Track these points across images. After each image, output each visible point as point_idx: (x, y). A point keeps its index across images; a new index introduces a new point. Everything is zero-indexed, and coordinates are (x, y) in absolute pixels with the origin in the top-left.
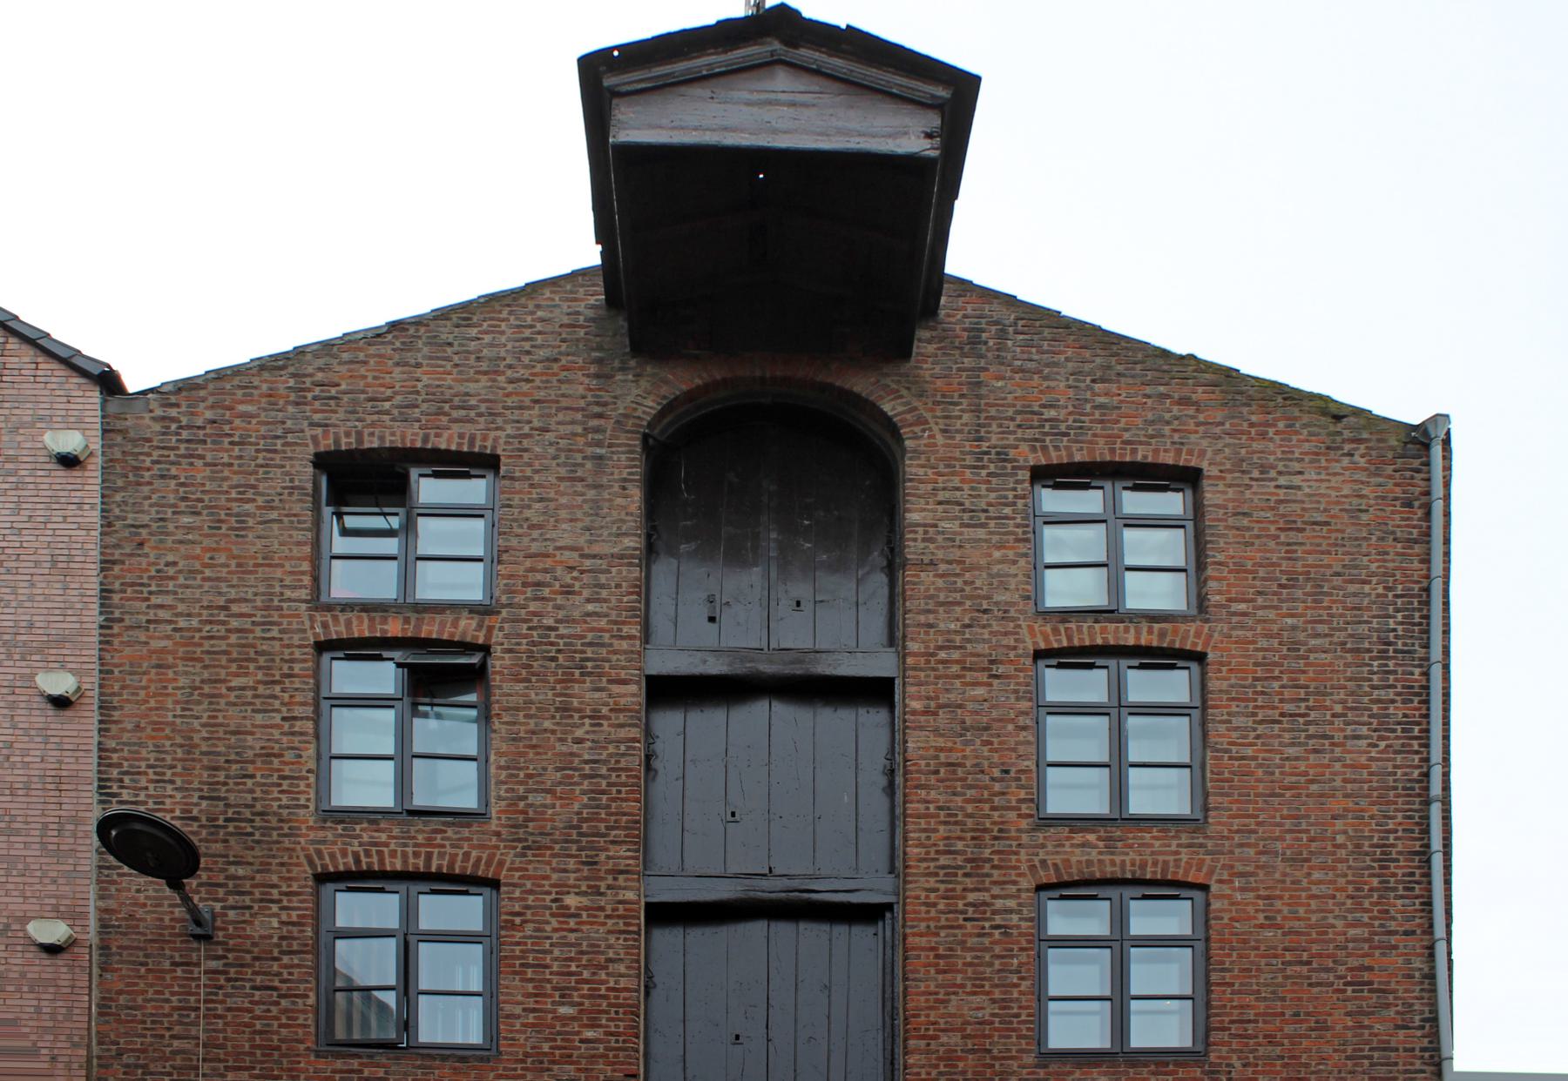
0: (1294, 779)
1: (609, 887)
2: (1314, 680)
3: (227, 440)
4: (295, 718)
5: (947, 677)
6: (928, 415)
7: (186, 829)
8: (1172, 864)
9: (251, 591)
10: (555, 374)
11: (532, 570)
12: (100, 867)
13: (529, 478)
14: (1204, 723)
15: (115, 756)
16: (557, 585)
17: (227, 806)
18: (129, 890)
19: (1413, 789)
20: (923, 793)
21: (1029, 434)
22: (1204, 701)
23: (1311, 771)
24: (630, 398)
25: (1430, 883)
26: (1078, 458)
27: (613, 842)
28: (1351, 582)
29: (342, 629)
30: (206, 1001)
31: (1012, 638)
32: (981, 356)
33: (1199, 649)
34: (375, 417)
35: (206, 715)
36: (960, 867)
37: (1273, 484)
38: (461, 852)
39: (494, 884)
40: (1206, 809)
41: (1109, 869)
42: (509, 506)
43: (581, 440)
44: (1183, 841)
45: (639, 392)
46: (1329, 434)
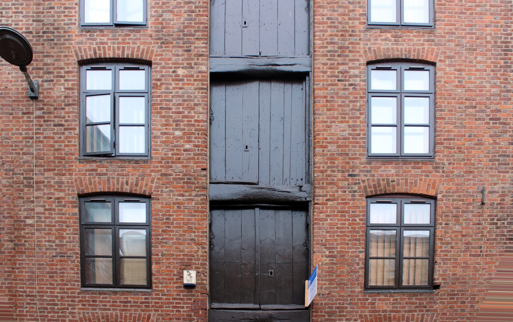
1: (196, 64)
7: (28, 38)
8: (421, 51)
18: (5, 73)
20: (321, 10)
27: (197, 39)
40: (435, 21)
41: (396, 53)
44: (426, 38)
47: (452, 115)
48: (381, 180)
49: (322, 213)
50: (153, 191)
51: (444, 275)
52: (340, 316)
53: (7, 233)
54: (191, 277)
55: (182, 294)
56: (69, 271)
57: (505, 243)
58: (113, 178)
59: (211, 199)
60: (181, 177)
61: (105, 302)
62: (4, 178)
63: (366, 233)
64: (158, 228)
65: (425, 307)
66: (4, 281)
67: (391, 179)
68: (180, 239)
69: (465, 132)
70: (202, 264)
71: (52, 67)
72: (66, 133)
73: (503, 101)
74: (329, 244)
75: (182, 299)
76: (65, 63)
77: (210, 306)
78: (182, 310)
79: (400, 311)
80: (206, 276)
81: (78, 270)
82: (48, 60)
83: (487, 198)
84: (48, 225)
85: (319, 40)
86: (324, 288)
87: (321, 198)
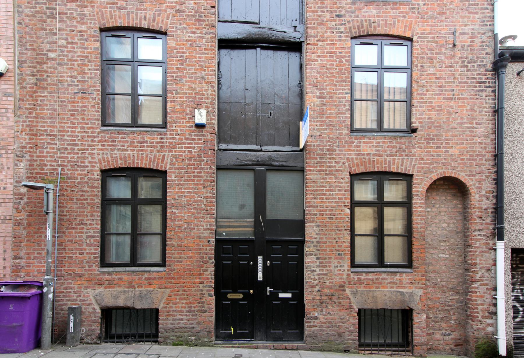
48: (364, 21)
49: (313, 53)
50: (168, 27)
53: (29, 67)
54: (201, 116)
55: (193, 133)
56: (90, 109)
57: (476, 87)
58: (132, 13)
59: (219, 38)
60: (193, 14)
61: (124, 142)
62: (27, 7)
63: (351, 75)
65: (405, 151)
66: (25, 119)
67: (372, 20)
74: (320, 85)
75: (193, 139)
78: (193, 150)
80: (214, 116)
81: (98, 108)
83: (458, 40)
84: (70, 60)
86: (315, 129)
87: (312, 38)
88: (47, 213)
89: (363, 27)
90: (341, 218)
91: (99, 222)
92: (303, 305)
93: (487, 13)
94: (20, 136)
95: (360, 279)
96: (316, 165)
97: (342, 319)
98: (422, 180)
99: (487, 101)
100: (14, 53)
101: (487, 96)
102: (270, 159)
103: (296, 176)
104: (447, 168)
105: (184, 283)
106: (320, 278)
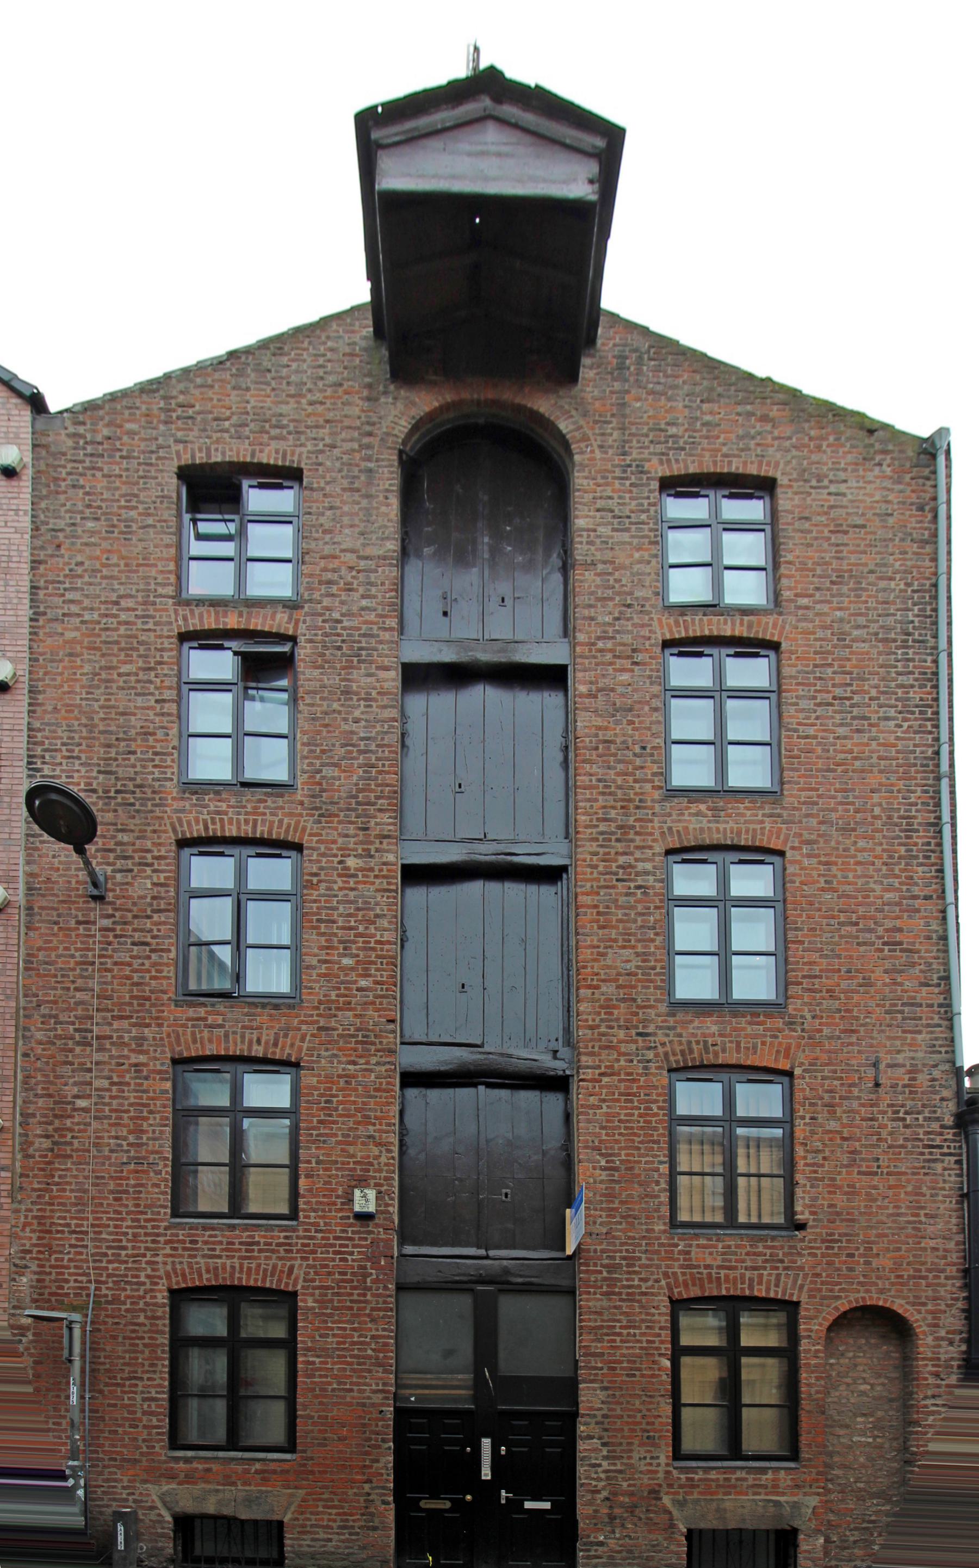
0: (843, 756)
1: (377, 850)
2: (856, 667)
3: (118, 454)
4: (164, 701)
5: (603, 664)
6: (590, 433)
7: (89, 800)
9: (134, 587)
10: (339, 397)
11: (325, 570)
12: (27, 835)
13: (323, 489)
14: (779, 706)
15: (39, 735)
16: (342, 582)
17: (117, 779)
19: (927, 765)
21: (660, 448)
22: (779, 685)
23: (856, 749)
24: (391, 418)
25: (942, 852)
26: (691, 470)
27: (380, 810)
28: (881, 578)
29: (197, 621)
30: (100, 956)
31: (647, 629)
32: (626, 380)
33: (776, 639)
34: (219, 435)
35: (103, 698)
36: (613, 833)
37: (826, 491)
38: (276, 819)
39: (298, 848)
40: (782, 783)
41: (715, 836)
42: (310, 513)
43: (357, 456)
44: (767, 811)
45: (397, 413)
46: (866, 446)
47: (815, 936)
51: (814, 1206)
52: (629, 1273)
53: (40, 1123)
54: (367, 1201)
57: (922, 1154)
61: (214, 1243)
62: (40, 1029)
64: (311, 1116)
65: (782, 1261)
66: (30, 1206)
67: (710, 1040)
68: (349, 1136)
69: (840, 964)
70: (386, 1179)
71: (131, 848)
72: (154, 956)
73: (906, 914)
74: (606, 1148)
76: (153, 844)
77: (399, 1251)
78: (349, 1257)
79: (735, 1268)
80: (392, 1199)
82: (125, 838)
84: (116, 1111)
85: (584, 814)
88: (70, 1361)
89: (691, 1051)
90: (653, 1376)
91: (167, 1376)
92: (576, 1522)
93: (940, 1032)
94: (21, 1234)
95: (692, 1479)
96: (599, 1284)
97: (654, 1546)
98: (819, 1311)
99: (947, 1178)
100: (14, 1102)
101: (945, 1169)
102: (506, 1271)
103: (558, 1303)
104: (867, 1291)
105: (333, 1481)
106: (608, 1478)
